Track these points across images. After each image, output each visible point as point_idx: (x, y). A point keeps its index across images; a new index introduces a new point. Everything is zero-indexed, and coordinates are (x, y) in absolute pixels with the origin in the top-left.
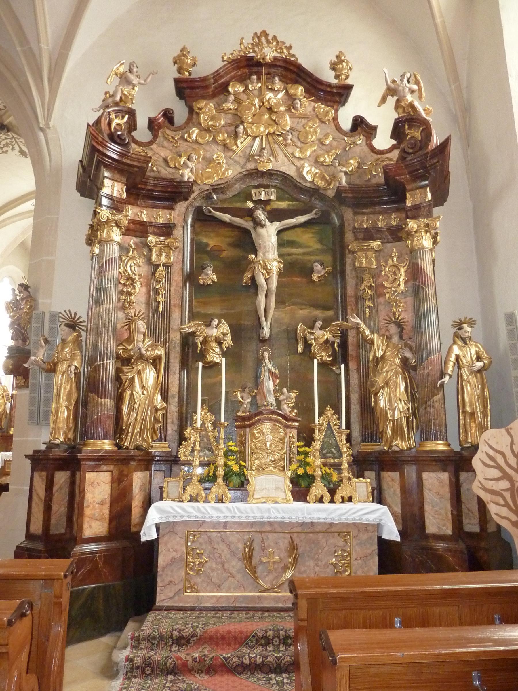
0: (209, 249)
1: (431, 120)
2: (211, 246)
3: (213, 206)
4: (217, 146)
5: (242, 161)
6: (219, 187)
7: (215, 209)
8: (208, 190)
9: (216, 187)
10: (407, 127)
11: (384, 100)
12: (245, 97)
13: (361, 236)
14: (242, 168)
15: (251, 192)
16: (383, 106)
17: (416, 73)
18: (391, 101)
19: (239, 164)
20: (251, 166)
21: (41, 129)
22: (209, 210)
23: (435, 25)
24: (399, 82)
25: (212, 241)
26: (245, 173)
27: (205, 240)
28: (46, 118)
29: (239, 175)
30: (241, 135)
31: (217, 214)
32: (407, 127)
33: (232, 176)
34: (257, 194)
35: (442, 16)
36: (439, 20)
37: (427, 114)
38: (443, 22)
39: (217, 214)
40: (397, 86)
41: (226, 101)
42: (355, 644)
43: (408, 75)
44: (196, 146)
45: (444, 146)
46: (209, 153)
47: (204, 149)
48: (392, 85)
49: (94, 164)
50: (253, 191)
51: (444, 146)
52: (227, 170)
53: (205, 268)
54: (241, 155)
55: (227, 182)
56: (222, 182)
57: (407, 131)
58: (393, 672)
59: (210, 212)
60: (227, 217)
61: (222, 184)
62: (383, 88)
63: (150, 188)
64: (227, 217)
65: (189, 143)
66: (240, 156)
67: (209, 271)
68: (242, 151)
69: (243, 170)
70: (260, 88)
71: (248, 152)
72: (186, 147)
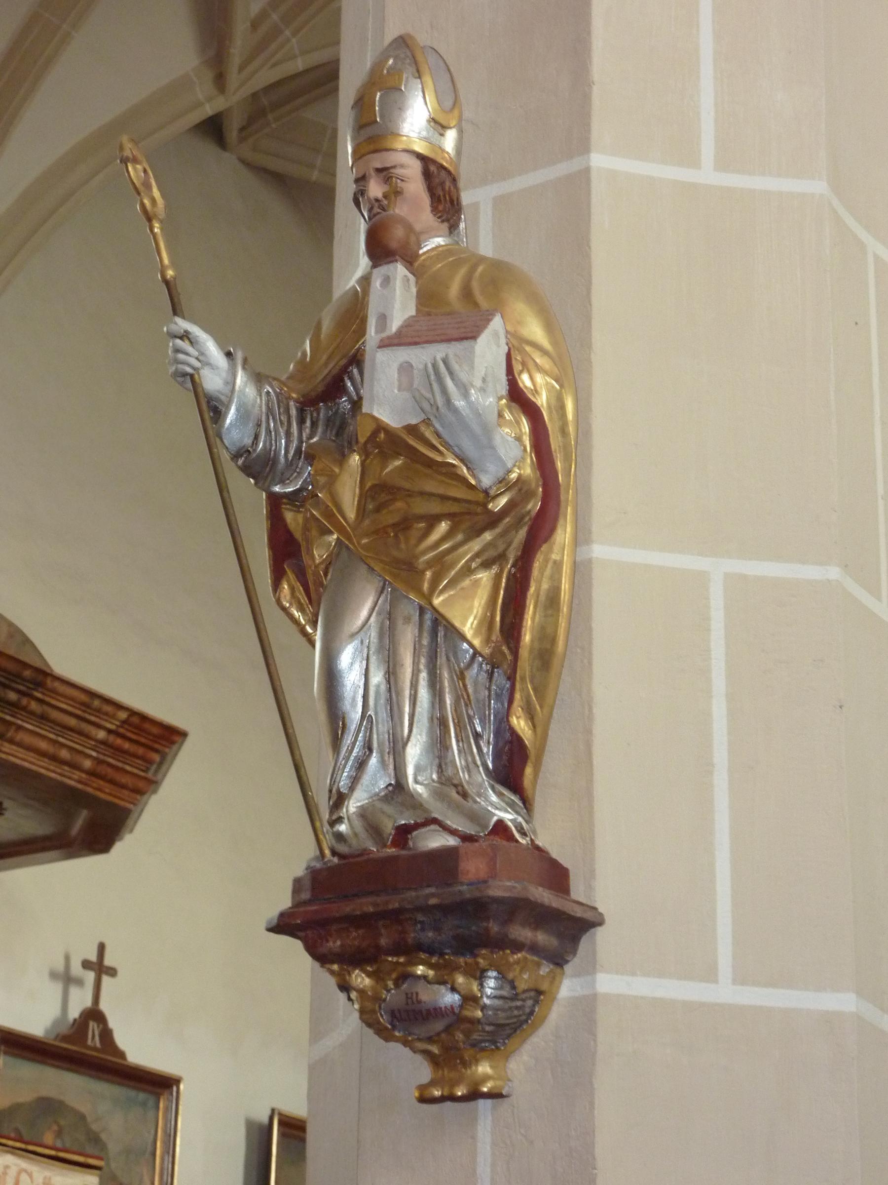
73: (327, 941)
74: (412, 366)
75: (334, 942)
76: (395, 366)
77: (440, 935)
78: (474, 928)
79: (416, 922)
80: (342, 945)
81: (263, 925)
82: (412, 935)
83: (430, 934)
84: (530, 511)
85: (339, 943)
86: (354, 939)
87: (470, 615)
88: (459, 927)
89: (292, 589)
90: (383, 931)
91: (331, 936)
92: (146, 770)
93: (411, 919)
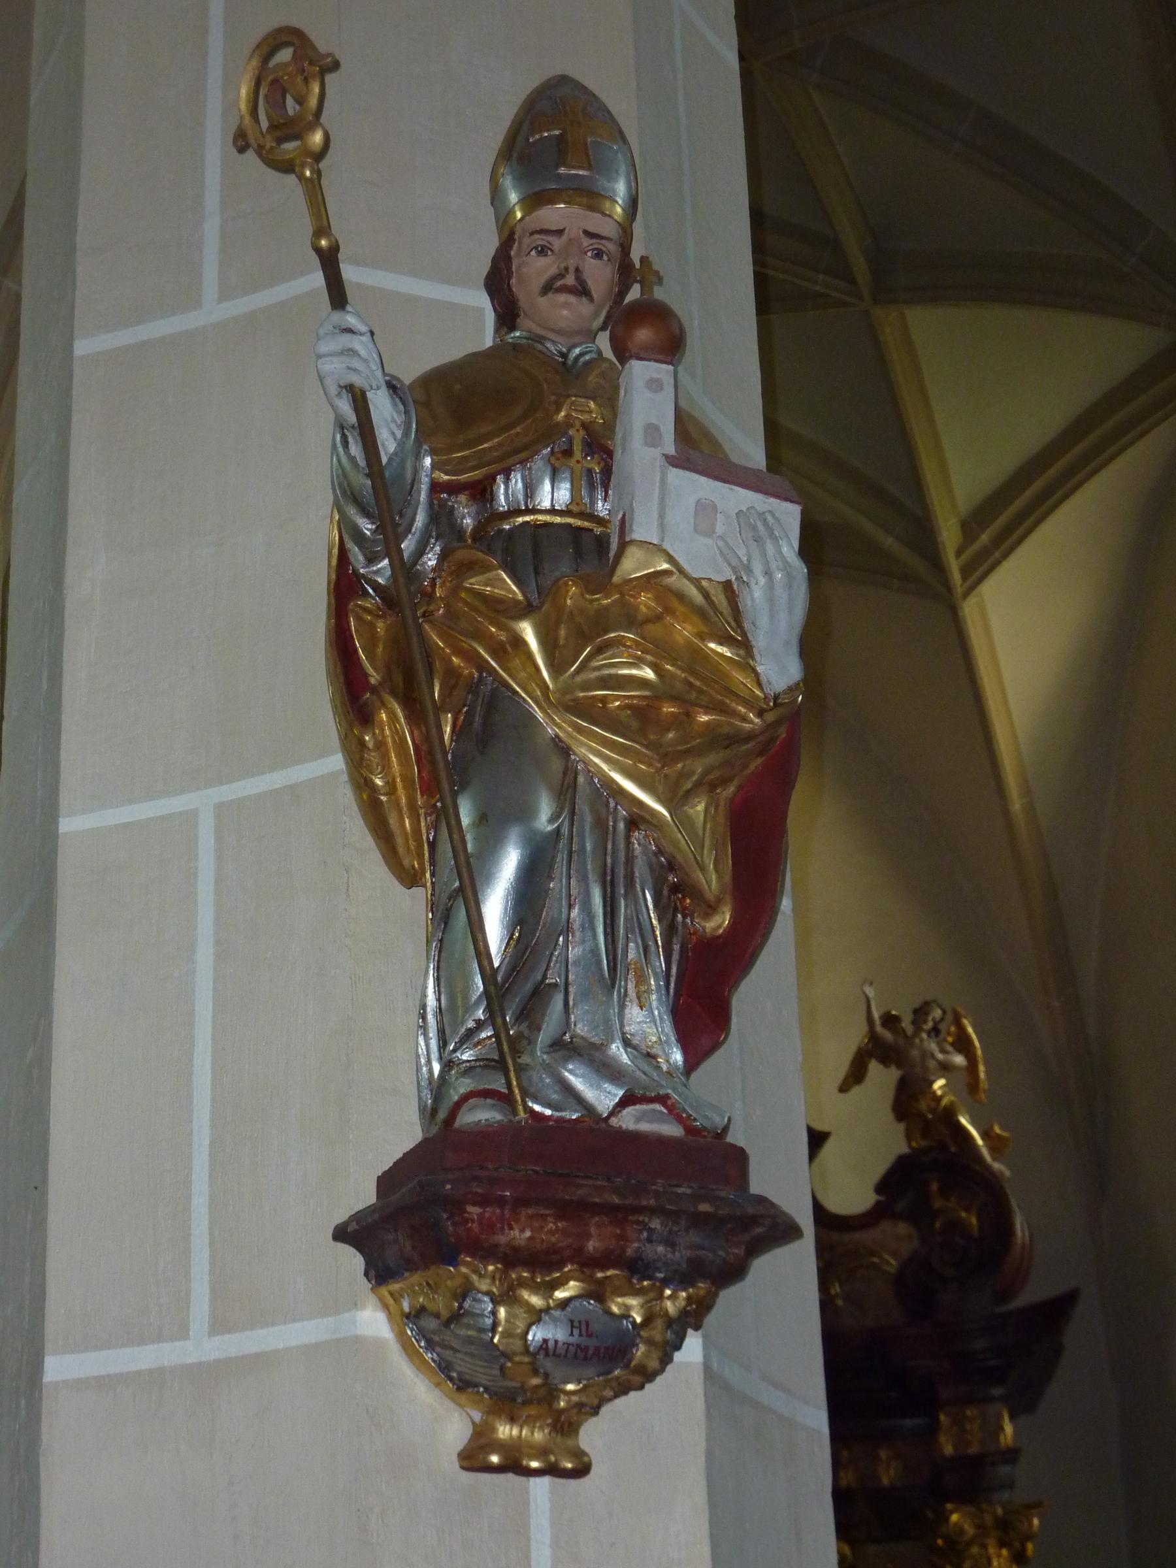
1: (1007, 1173)
10: (934, 1186)
11: (856, 1075)
13: (592, 379)
16: (856, 1091)
17: (960, 1010)
18: (881, 1079)
23: (1006, 813)
24: (907, 1025)
32: (934, 1186)
35: (1026, 790)
36: (1017, 805)
37: (993, 1150)
38: (1030, 807)
40: (901, 1041)
42: (467, 1354)
43: (937, 1013)
45: (1059, 1309)
48: (887, 1035)
51: (1059, 1309)
57: (938, 1204)
58: (401, 407)
62: (854, 1036)
73: (511, 1228)
74: (715, 507)
75: (522, 1231)
76: (692, 502)
77: (674, 1253)
78: (721, 1253)
79: (645, 1226)
80: (531, 1238)
81: (835, 1091)
82: (636, 1245)
83: (660, 1249)
84: (1023, 1243)
85: (528, 1234)
86: (551, 1232)
87: (617, 675)
88: (699, 1247)
89: (708, 883)
90: (593, 1230)
91: (518, 1220)
92: (585, 994)
93: (638, 1222)
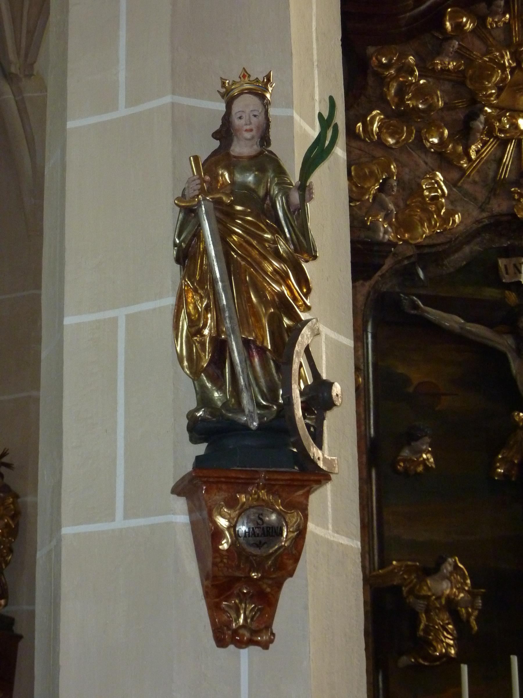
0: (411, 390)
2: (415, 382)
3: (422, 292)
4: (423, 156)
5: (481, 194)
6: (434, 250)
7: (429, 301)
8: (411, 257)
9: (426, 250)
12: (478, 43)
14: (482, 209)
15: (497, 263)
19: (475, 199)
20: (499, 206)
21: (9, 77)
22: (413, 302)
25: (416, 374)
26: (486, 222)
27: (401, 369)
28: (23, 52)
29: (475, 226)
30: (478, 135)
31: (433, 314)
33: (461, 228)
34: (511, 270)
39: (433, 314)
41: (439, 53)
44: (378, 153)
46: (407, 170)
47: (396, 161)
49: (253, 229)
50: (502, 262)
52: (450, 214)
53: (417, 439)
54: (477, 179)
55: (450, 242)
56: (441, 240)
59: (416, 307)
60: (452, 321)
61: (439, 245)
63: (292, 247)
64: (452, 321)
65: (362, 145)
66: (475, 182)
67: (425, 444)
68: (478, 171)
69: (485, 215)
70: (508, 25)
71: (491, 174)
72: (357, 151)
